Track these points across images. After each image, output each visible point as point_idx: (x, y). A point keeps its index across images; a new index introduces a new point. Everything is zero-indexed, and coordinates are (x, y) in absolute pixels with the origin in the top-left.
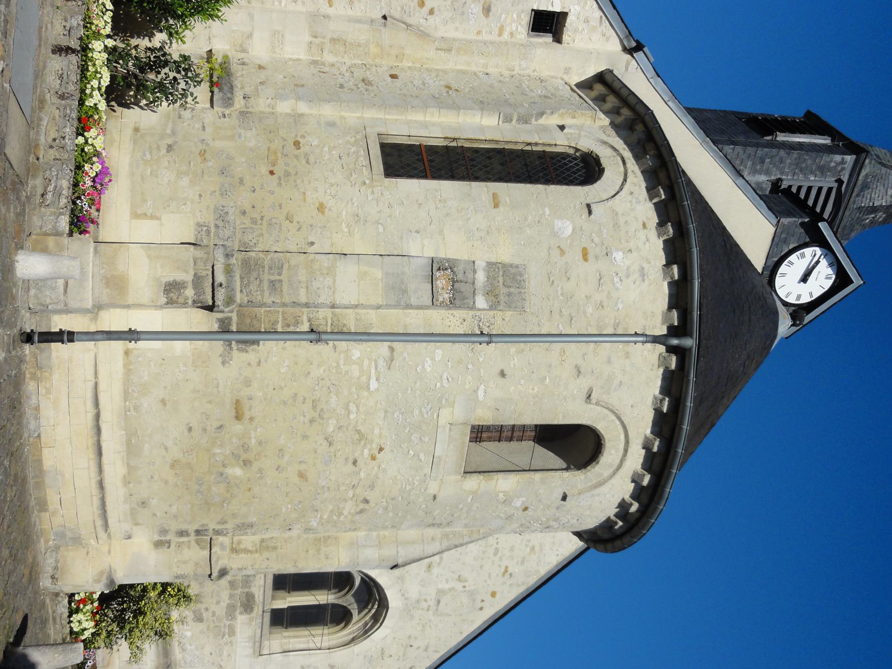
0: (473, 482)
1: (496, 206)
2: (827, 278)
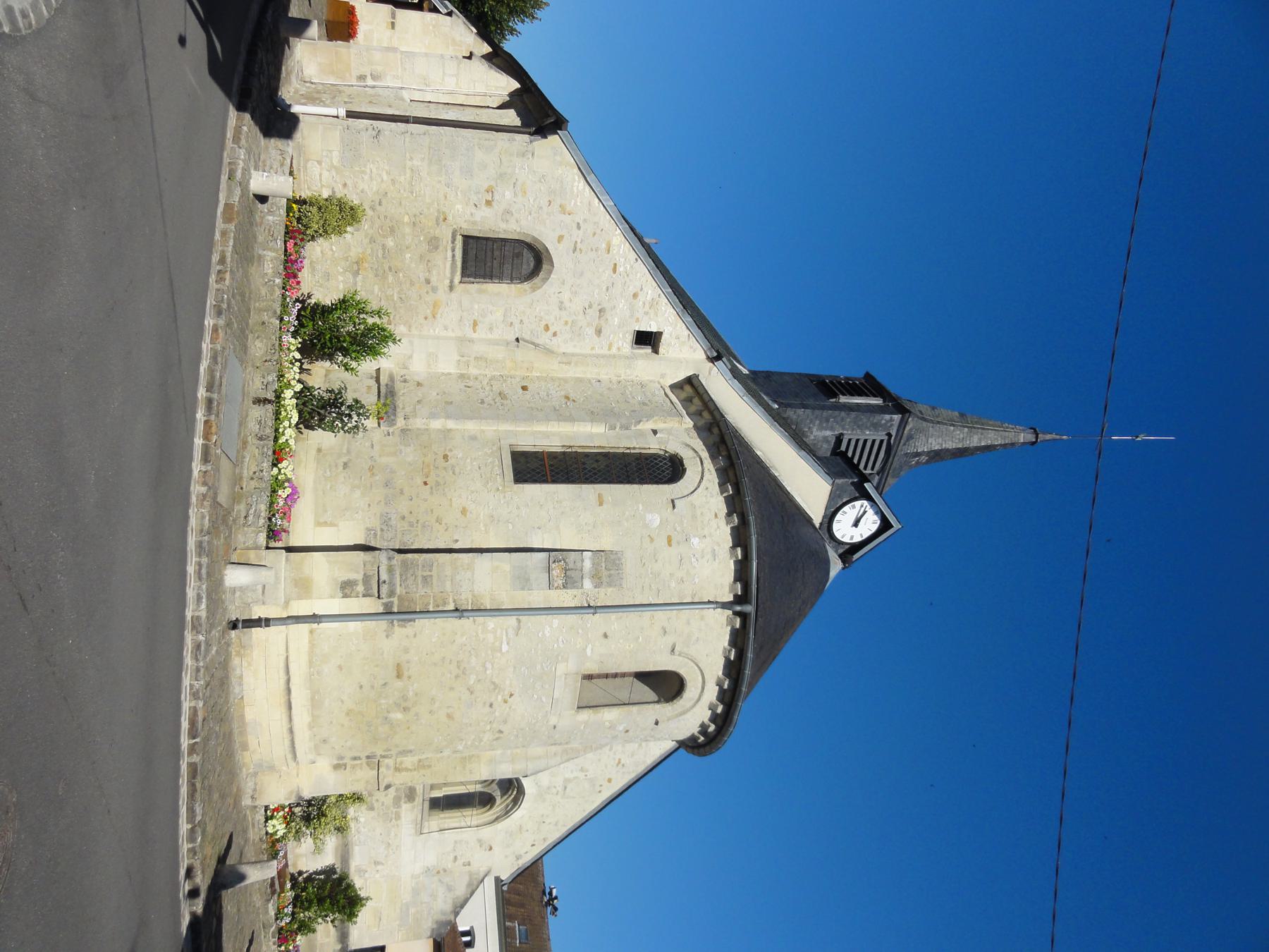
0: (585, 715)
1: (601, 504)
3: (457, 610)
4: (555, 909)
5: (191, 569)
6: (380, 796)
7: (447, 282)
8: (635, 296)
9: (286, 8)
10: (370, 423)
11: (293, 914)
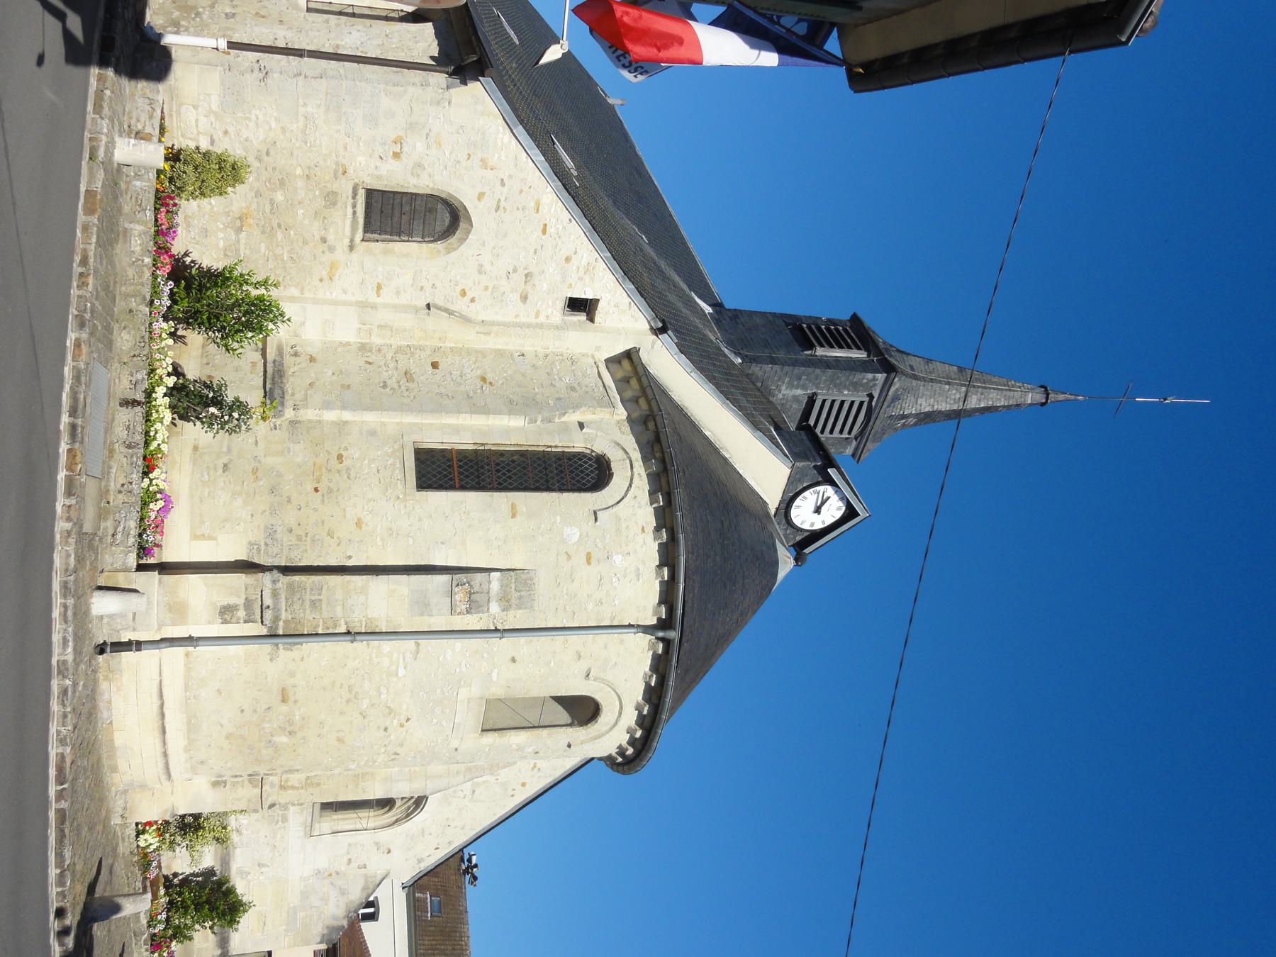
0: (491, 738)
1: (514, 516)
2: (839, 509)
3: (349, 633)
4: (475, 878)
5: (56, 614)
7: (347, 242)
8: (568, 259)
11: (168, 920)
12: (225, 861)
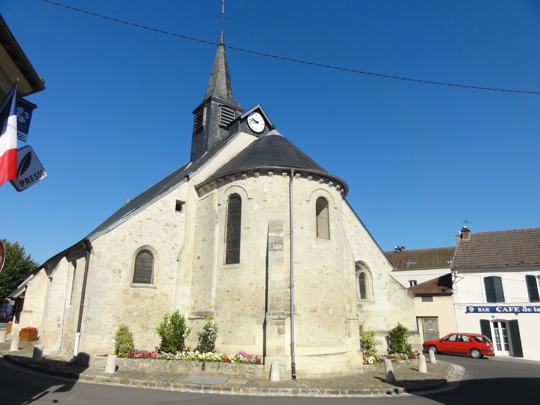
0: (332, 236)
1: (249, 228)
3: (290, 288)
4: (403, 247)
5: (273, 394)
6: (360, 318)
7: (153, 290)
8: (161, 211)
9: (28, 359)
10: (213, 322)
11: (403, 353)
12: (382, 332)
